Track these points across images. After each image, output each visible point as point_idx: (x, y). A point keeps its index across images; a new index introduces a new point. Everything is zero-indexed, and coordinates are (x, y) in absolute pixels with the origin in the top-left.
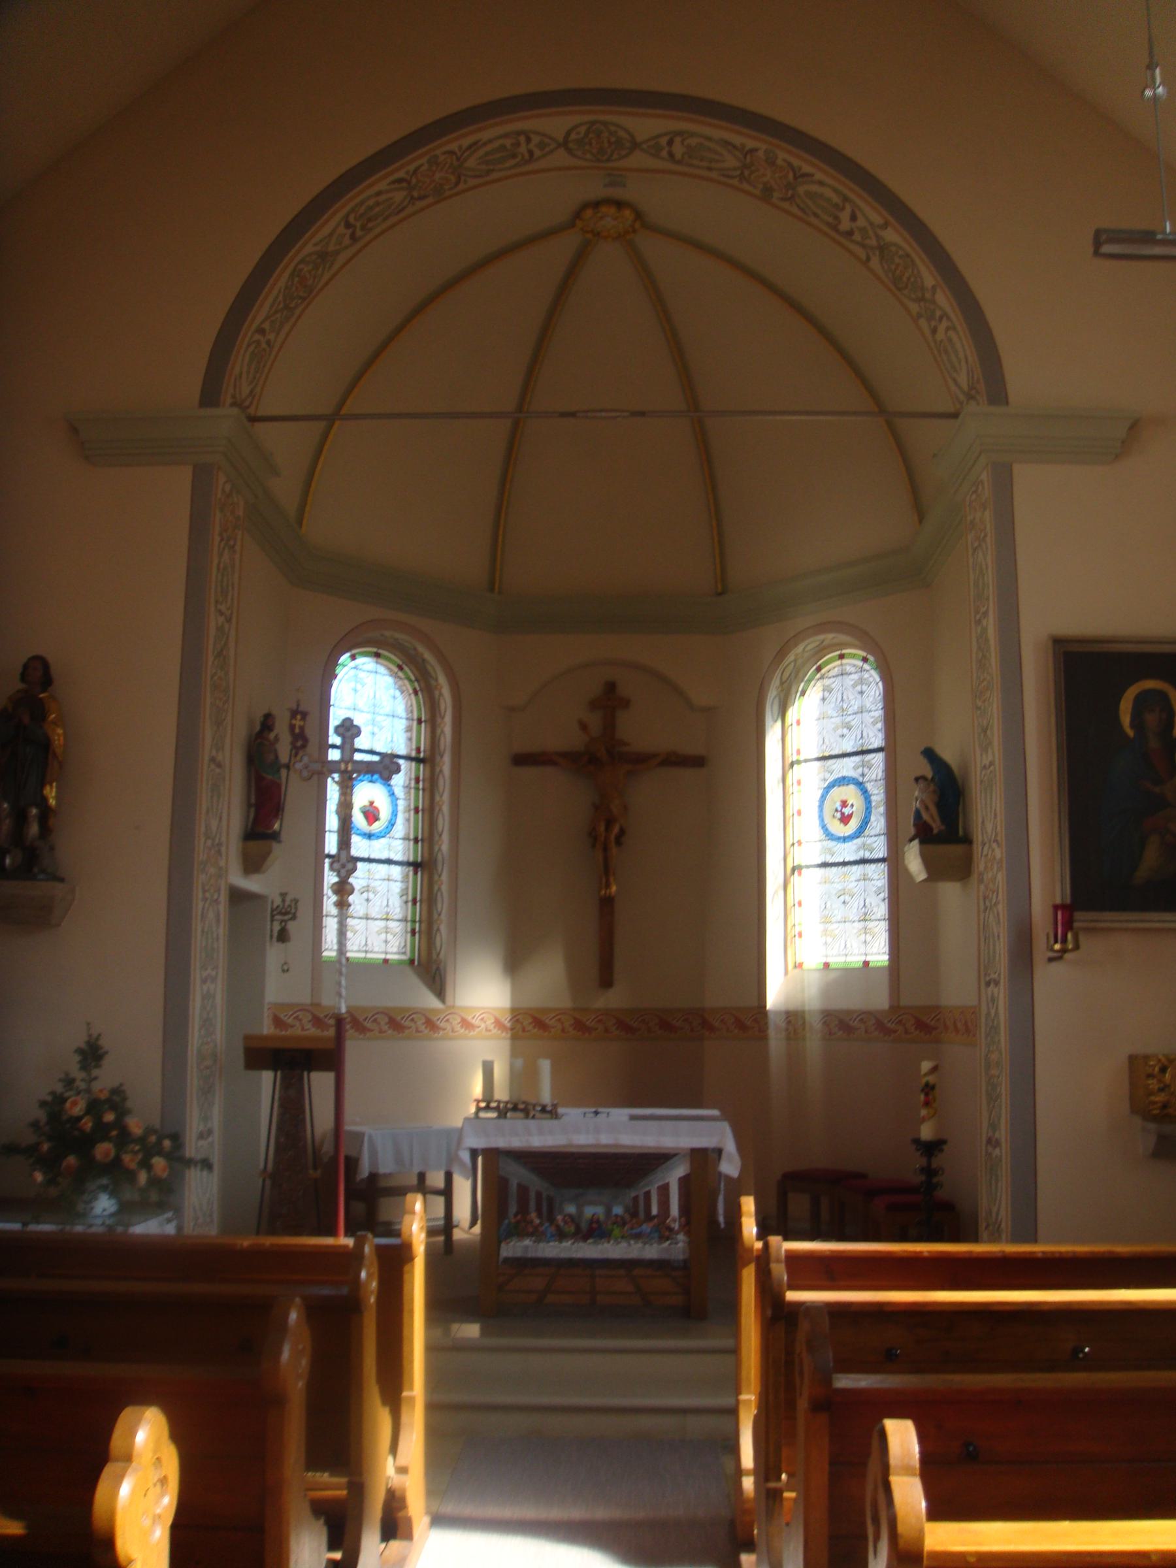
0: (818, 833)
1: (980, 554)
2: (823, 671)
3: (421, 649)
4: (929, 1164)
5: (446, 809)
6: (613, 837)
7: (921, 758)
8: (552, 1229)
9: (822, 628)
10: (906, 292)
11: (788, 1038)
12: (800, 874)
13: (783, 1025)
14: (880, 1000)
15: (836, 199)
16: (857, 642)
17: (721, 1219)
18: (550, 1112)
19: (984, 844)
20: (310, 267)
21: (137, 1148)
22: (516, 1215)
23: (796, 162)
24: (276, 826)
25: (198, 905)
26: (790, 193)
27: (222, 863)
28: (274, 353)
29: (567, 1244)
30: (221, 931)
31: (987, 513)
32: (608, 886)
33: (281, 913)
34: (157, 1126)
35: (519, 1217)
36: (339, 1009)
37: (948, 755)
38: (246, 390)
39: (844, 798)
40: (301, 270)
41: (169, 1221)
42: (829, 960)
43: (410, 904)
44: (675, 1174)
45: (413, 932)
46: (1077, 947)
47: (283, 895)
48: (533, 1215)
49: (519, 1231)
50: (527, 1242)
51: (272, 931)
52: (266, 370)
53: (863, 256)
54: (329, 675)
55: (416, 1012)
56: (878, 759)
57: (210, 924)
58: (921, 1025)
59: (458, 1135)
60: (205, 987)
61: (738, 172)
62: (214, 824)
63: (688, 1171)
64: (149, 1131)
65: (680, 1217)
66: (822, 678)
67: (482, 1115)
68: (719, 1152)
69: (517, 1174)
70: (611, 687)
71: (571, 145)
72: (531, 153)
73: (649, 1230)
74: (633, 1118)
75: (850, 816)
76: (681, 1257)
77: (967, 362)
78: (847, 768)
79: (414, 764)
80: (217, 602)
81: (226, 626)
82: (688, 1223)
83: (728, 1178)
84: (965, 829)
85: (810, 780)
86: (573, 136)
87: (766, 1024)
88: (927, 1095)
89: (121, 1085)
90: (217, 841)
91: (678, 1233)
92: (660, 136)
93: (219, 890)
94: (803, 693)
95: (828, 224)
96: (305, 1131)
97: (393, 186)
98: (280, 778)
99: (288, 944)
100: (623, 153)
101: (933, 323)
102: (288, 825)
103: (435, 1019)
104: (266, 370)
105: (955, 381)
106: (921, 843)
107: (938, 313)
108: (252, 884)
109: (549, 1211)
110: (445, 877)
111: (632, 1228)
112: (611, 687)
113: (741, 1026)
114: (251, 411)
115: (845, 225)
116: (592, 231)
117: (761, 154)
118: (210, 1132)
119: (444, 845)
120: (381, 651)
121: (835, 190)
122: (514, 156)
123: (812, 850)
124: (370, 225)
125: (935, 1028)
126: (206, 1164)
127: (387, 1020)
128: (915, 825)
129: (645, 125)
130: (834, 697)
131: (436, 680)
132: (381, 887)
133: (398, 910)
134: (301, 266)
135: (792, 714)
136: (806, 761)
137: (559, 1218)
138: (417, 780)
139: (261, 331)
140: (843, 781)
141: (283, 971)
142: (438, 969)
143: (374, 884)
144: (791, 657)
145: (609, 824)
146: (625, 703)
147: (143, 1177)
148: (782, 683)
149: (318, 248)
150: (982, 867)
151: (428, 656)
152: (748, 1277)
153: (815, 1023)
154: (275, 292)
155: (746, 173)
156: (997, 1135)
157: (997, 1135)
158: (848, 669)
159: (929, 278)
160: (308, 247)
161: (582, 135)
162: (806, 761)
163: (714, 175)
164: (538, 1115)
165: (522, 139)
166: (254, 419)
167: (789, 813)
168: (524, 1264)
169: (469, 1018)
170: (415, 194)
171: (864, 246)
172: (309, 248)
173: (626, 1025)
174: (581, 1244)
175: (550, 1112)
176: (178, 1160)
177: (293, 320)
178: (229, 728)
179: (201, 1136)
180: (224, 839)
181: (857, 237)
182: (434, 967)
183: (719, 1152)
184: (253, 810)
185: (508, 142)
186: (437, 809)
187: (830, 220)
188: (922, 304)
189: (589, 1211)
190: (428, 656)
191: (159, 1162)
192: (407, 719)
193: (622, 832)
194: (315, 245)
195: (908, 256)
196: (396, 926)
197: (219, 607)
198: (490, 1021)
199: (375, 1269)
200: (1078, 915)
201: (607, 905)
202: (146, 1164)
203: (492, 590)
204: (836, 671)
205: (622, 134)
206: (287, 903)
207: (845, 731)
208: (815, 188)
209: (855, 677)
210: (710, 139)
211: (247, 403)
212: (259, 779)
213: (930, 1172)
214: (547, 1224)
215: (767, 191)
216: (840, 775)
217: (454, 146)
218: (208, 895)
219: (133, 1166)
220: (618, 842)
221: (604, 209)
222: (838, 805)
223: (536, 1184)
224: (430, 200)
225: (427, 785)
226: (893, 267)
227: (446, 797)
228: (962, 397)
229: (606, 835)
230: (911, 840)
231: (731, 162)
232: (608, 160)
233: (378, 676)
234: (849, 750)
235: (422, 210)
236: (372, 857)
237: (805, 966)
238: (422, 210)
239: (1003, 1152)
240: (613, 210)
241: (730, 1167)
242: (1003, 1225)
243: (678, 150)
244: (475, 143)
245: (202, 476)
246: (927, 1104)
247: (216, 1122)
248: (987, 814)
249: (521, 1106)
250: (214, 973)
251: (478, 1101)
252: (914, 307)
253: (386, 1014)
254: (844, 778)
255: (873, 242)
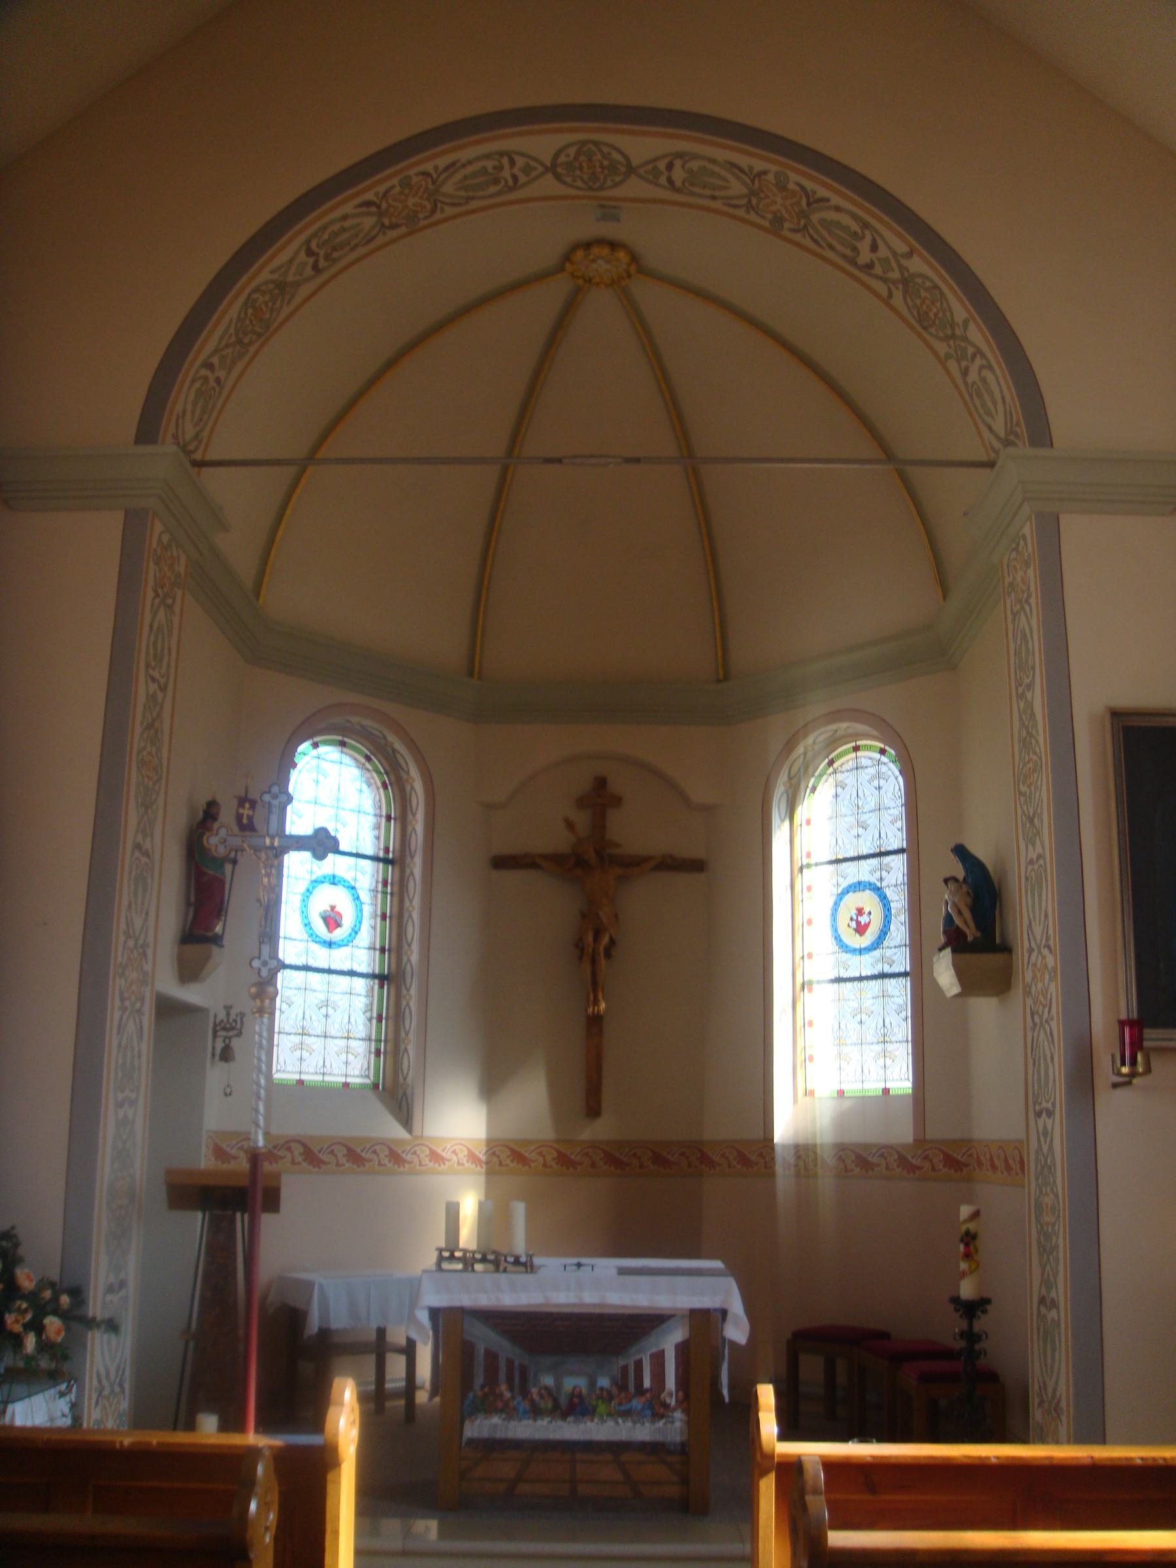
0: (830, 945)
1: (1023, 618)
2: (835, 765)
3: (391, 737)
4: (971, 1326)
5: (416, 915)
6: (602, 949)
7: (952, 856)
8: (525, 1405)
9: (835, 716)
10: (933, 331)
11: (798, 1175)
12: (810, 990)
13: (792, 1161)
14: (904, 1133)
15: (855, 227)
16: (875, 733)
17: (725, 1392)
18: (525, 1265)
19: (1031, 950)
20: (267, 298)
21: (24, 1305)
22: (483, 1387)
23: (809, 185)
24: (218, 929)
25: (114, 1014)
26: (803, 222)
27: (148, 967)
28: (225, 394)
29: (543, 1422)
30: (144, 1047)
31: (1031, 572)
32: (596, 1002)
33: (224, 1029)
34: (55, 1275)
35: (486, 1389)
36: (256, 1142)
37: (980, 850)
38: (190, 432)
39: (860, 905)
40: (255, 301)
41: (62, 1394)
42: (844, 1087)
43: (374, 1021)
44: (671, 1340)
45: (378, 1053)
46: (1148, 1070)
47: (228, 1008)
48: (503, 1387)
49: (488, 1405)
50: (496, 1420)
51: (214, 1048)
52: (215, 414)
53: (885, 293)
54: (287, 763)
55: (382, 1142)
56: (898, 864)
57: (130, 1038)
58: (952, 1163)
59: (413, 1288)
60: (121, 1113)
61: (744, 201)
62: (138, 922)
63: (687, 1335)
64: (44, 1283)
65: (677, 1391)
66: (835, 772)
67: (446, 1266)
68: (724, 1313)
69: (484, 1338)
70: (601, 783)
71: (559, 170)
72: (515, 178)
73: (640, 1407)
74: (623, 1271)
75: (867, 925)
76: (678, 1439)
77: (1004, 402)
78: (864, 871)
79: (381, 865)
80: (148, 666)
81: (160, 695)
82: (687, 1397)
83: (734, 1345)
84: (1002, 935)
85: (822, 885)
86: (562, 159)
87: (773, 1158)
88: (967, 1245)
89: (13, 1228)
90: (141, 942)
91: (674, 1409)
92: (657, 159)
93: (143, 1000)
94: (814, 790)
95: (844, 257)
96: (235, 1285)
97: (360, 210)
98: (223, 874)
99: (232, 1064)
100: (617, 179)
101: (964, 364)
102: (235, 927)
103: (400, 1152)
104: (215, 414)
105: (990, 428)
106: (954, 951)
107: (971, 350)
108: (191, 995)
109: (522, 1381)
110: (413, 991)
111: (620, 1404)
112: (601, 783)
113: (744, 1160)
114: (198, 456)
115: (865, 256)
116: (583, 277)
117: (770, 177)
118: (123, 1284)
119: (414, 956)
120: (346, 740)
121: (855, 217)
122: (496, 181)
123: (823, 961)
124: (335, 255)
125: (967, 1165)
126: (112, 1326)
127: (301, 1149)
128: (945, 932)
129: (641, 146)
130: (847, 795)
131: (408, 773)
132: (342, 1001)
133: (361, 1027)
134: (255, 296)
135: (801, 813)
136: (816, 865)
137: (534, 1390)
138: (385, 883)
139: (210, 366)
140: (858, 886)
141: (226, 1095)
142: (405, 1093)
143: (333, 998)
144: (800, 749)
145: (597, 935)
146: (617, 801)
147: (30, 1342)
148: (790, 778)
149: (276, 276)
150: (1029, 977)
151: (399, 746)
152: (767, 1488)
153: (828, 1157)
154: (225, 321)
155: (754, 201)
156: (1053, 1294)
157: (1053, 1294)
158: (864, 762)
159: (959, 310)
160: (263, 273)
161: (571, 158)
162: (816, 865)
163: (717, 205)
164: (510, 1268)
165: (505, 161)
166: (200, 464)
167: (798, 922)
168: (492, 1446)
169: (439, 1151)
170: (386, 222)
171: (885, 280)
172: (265, 275)
173: (616, 1159)
174: (560, 1423)
175: (525, 1265)
176: (77, 1318)
177: (247, 358)
178: (161, 812)
179: (110, 1289)
180: (151, 939)
181: (878, 270)
182: (401, 1092)
183: (724, 1313)
184: (192, 909)
185: (489, 164)
186: (406, 915)
187: (848, 252)
188: (951, 342)
189: (571, 1383)
190: (399, 746)
191: (52, 1323)
192: (375, 815)
193: (612, 942)
194: (273, 272)
195: (936, 287)
196: (360, 1047)
197: (151, 672)
198: (463, 1154)
199: (274, 1497)
200: (1148, 1033)
201: (595, 1023)
202: (37, 1326)
203: (471, 675)
204: (851, 765)
205: (616, 156)
206: (233, 1016)
207: (861, 831)
208: (831, 215)
209: (872, 771)
210: (713, 161)
211: (191, 447)
212: (200, 873)
213: (971, 1337)
214: (519, 1398)
215: (778, 220)
216: (856, 880)
217: (429, 167)
218: (127, 1004)
219: (18, 1328)
220: (608, 954)
221: (596, 250)
222: (853, 913)
223: (506, 1348)
224: (404, 230)
225: (396, 889)
226: (918, 302)
227: (416, 902)
228: (997, 445)
229: (594, 948)
230: (940, 950)
231: (737, 188)
232: (601, 188)
233: (343, 767)
234: (865, 851)
235: (393, 241)
236: (333, 967)
237: (816, 1094)
238: (393, 241)
239: (1062, 1315)
240: (606, 251)
241: (737, 1331)
242: (1063, 1404)
243: (678, 175)
244: (454, 164)
245: (135, 524)
246: (968, 1256)
247: (131, 1272)
248: (1033, 917)
249: (491, 1257)
250: (133, 1096)
251: (440, 1250)
252: (942, 348)
253: (346, 1146)
254: (859, 883)
255: (895, 275)
